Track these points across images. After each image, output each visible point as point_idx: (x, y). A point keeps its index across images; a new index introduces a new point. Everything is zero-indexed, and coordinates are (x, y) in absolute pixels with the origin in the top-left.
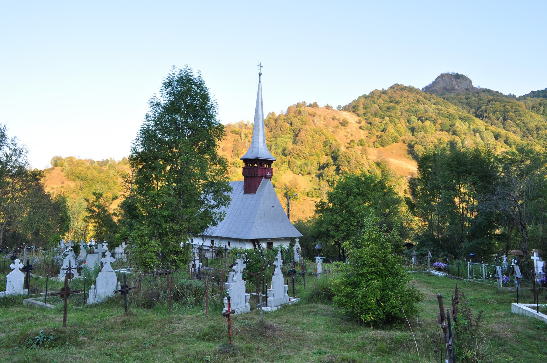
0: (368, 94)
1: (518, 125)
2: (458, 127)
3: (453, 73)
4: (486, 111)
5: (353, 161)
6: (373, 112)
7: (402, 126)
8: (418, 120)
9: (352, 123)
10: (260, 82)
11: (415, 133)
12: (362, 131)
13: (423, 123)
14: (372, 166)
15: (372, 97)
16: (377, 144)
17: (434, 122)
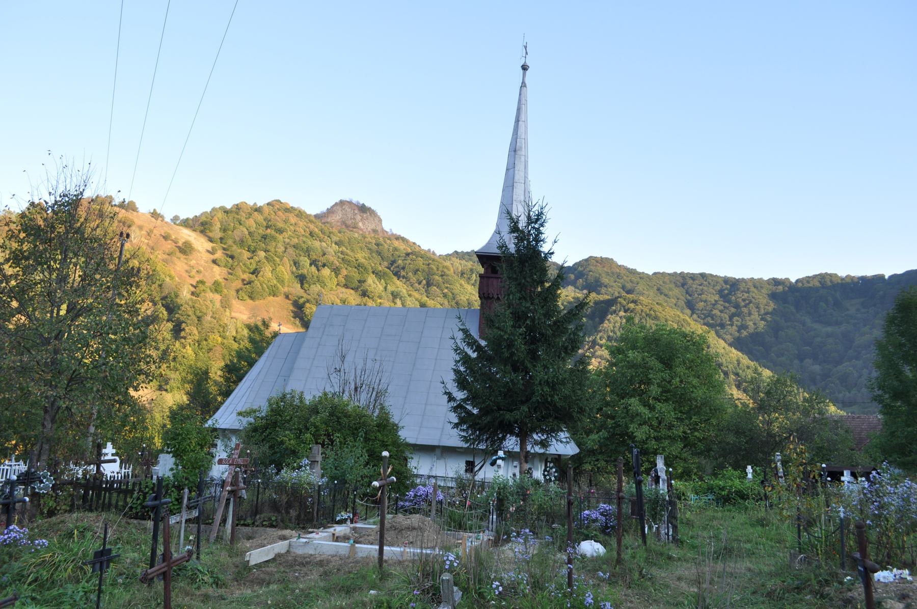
0: (229, 206)
1: (445, 296)
2: (370, 286)
3: (358, 202)
4: (403, 268)
5: (208, 318)
6: (238, 239)
7: (286, 270)
8: (311, 265)
9: (199, 251)
10: (523, 85)
11: (306, 286)
12: (216, 269)
13: (318, 270)
14: (240, 330)
15: (237, 213)
16: (243, 294)
17: (336, 271)
